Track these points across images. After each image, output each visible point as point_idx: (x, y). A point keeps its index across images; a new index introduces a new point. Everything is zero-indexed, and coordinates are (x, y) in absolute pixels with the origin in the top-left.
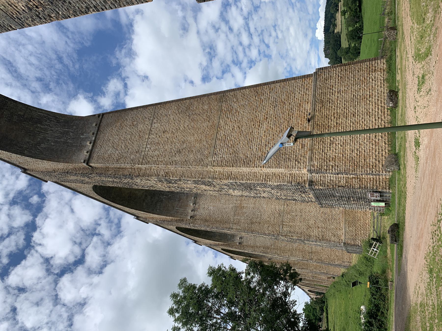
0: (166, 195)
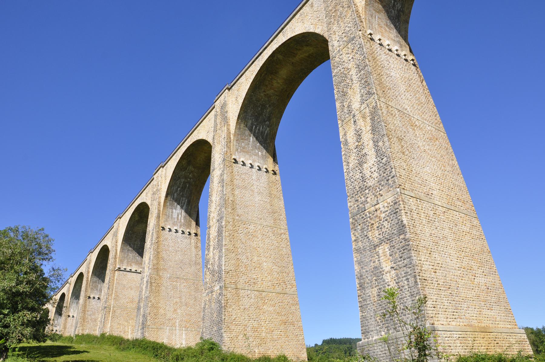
0: (394, 4)
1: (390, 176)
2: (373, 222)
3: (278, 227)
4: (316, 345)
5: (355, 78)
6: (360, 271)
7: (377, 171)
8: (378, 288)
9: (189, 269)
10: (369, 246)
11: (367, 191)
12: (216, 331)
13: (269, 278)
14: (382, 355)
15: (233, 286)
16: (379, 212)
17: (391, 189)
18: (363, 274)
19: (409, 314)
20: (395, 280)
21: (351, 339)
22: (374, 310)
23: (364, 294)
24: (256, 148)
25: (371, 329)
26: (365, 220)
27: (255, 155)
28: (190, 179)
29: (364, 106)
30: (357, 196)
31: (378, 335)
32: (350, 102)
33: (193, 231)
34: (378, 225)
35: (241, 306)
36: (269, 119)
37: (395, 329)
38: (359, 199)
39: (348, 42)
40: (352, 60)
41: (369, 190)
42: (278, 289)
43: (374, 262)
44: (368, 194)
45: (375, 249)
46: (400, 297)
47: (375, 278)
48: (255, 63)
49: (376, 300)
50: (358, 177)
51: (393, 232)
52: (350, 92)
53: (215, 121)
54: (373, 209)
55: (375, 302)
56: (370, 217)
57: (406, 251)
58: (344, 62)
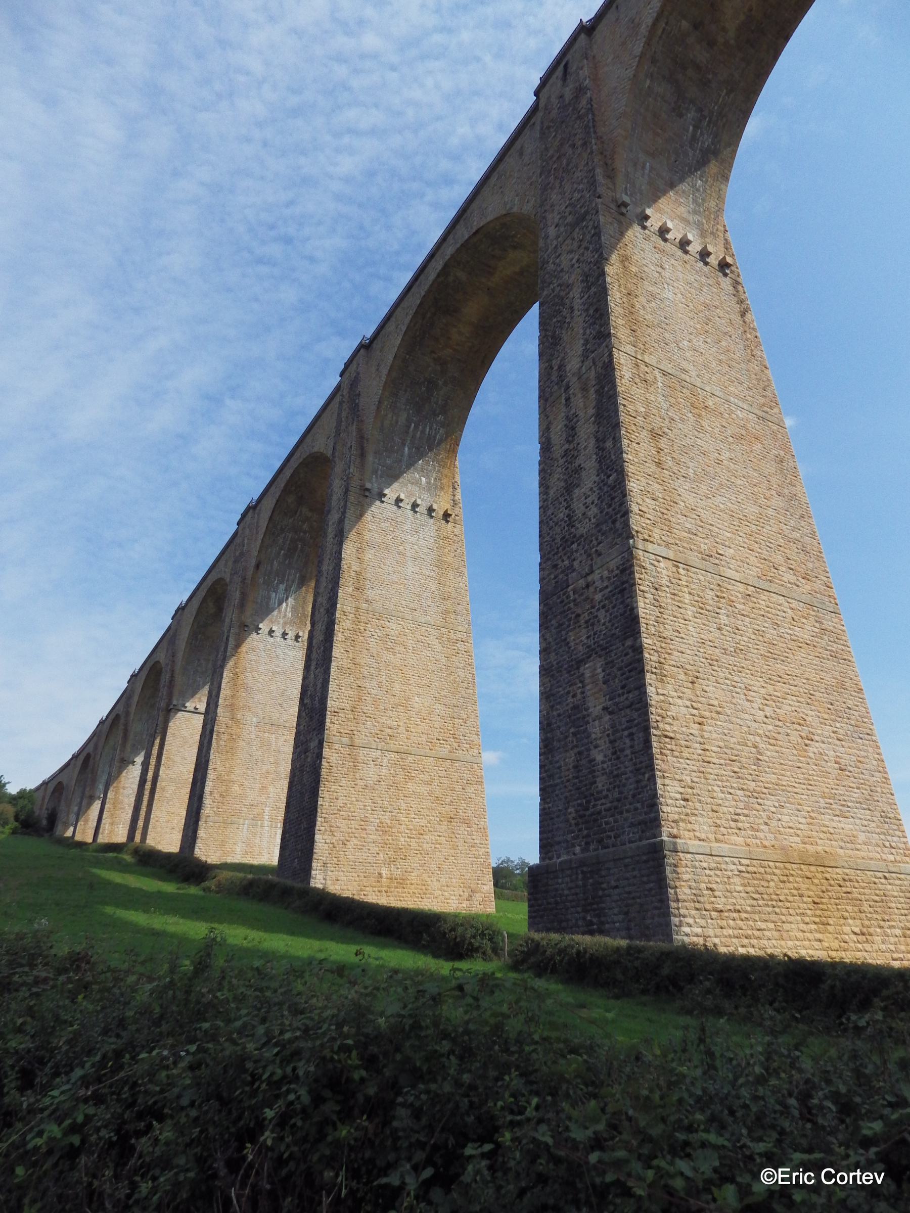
1: (619, 512)
2: (579, 611)
5: (578, 304)
6: (548, 713)
7: (596, 502)
8: (576, 750)
10: (568, 662)
11: (574, 546)
12: (305, 829)
13: (423, 727)
14: (570, 898)
15: (346, 740)
16: (591, 589)
17: (618, 540)
18: (554, 721)
19: (628, 811)
20: (608, 735)
22: (566, 798)
23: (551, 763)
25: (557, 839)
26: (566, 608)
28: (305, 532)
29: (589, 363)
30: (556, 557)
31: (568, 853)
32: (563, 359)
34: (587, 618)
35: (358, 782)
37: (600, 841)
38: (559, 562)
39: (573, 226)
40: (576, 265)
41: (579, 545)
42: (444, 751)
43: (574, 696)
44: (577, 551)
45: (578, 668)
46: (615, 773)
47: (572, 730)
48: (413, 290)
49: (571, 776)
50: (561, 515)
51: (613, 632)
52: (566, 336)
53: (339, 414)
54: (582, 583)
55: (568, 781)
56: (575, 600)
57: (633, 673)
58: (562, 270)
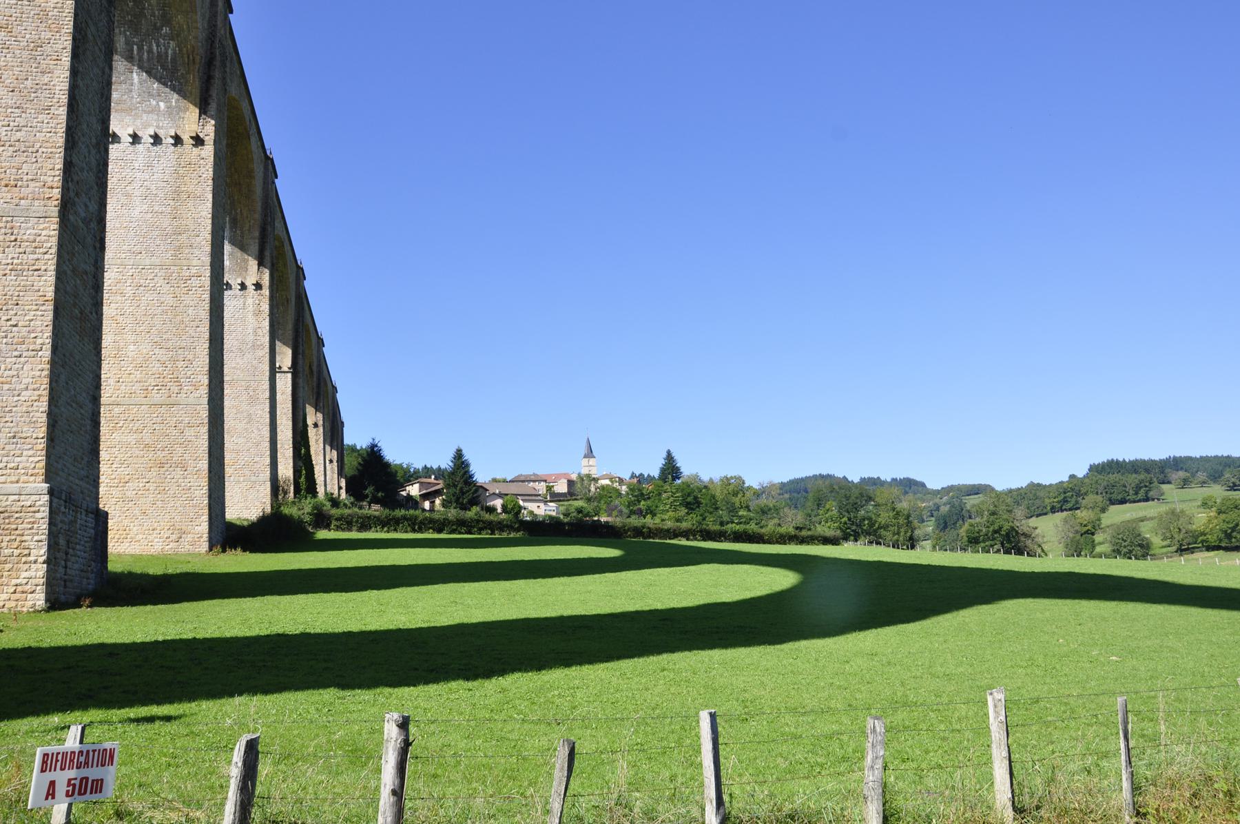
3: (185, 262)
4: (1072, 477)
9: (238, 360)
21: (1190, 458)
24: (150, 95)
27: (149, 112)
33: (250, 282)
36: (166, 20)
42: (157, 397)
